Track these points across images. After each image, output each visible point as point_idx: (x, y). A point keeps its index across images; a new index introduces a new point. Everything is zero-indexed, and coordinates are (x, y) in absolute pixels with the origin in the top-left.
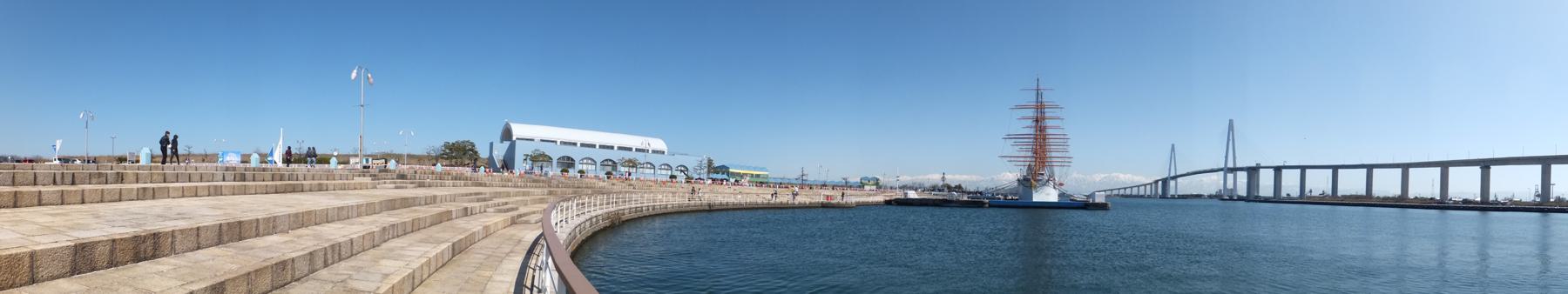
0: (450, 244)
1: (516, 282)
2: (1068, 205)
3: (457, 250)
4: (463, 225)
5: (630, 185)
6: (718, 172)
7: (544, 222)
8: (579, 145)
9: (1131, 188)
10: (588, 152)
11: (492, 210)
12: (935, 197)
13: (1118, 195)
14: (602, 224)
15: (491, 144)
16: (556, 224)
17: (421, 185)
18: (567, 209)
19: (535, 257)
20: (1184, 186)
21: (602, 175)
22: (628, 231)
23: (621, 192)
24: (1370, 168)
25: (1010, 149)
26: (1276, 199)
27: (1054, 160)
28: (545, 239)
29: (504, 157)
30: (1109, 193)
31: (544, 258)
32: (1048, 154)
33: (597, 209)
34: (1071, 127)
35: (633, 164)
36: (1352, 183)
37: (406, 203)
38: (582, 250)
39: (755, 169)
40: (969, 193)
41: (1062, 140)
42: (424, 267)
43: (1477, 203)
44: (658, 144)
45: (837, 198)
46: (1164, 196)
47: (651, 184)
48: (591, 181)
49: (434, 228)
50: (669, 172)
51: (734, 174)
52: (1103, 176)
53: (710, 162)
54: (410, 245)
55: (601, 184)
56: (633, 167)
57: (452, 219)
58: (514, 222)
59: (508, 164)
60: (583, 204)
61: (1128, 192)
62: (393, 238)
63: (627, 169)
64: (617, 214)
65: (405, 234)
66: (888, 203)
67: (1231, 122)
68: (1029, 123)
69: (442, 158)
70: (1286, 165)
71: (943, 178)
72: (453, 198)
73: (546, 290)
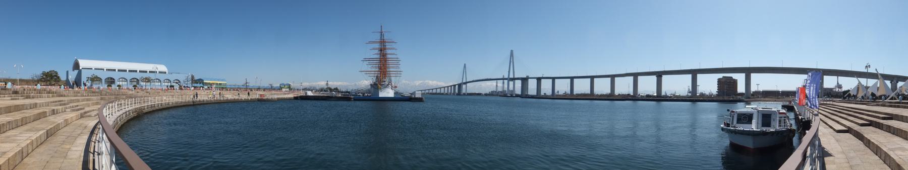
0: (45, 131)
1: (85, 150)
2: (400, 99)
3: (50, 134)
4: (52, 120)
5: (147, 92)
6: (197, 82)
7: (100, 114)
8: (117, 71)
9: (436, 89)
10: (122, 74)
11: (69, 110)
12: (322, 95)
13: (428, 93)
14: (132, 115)
15: (67, 72)
16: (106, 116)
17: (28, 97)
18: (112, 108)
19: (95, 135)
20: (471, 88)
21: (131, 87)
22: (146, 120)
23: (142, 97)
24: (592, 78)
25: (366, 67)
26: (538, 96)
27: (391, 73)
28: (101, 124)
29: (75, 80)
30: (423, 92)
31: (101, 135)
32: (388, 70)
33: (129, 107)
34: (399, 52)
35: (148, 80)
36: (582, 87)
37: (18, 108)
38: (122, 129)
39: (218, 80)
40: (342, 92)
42: (29, 146)
43: (654, 96)
44: (162, 68)
45: (269, 95)
46: (459, 94)
47: (159, 91)
48: (124, 91)
49: (35, 122)
50: (169, 84)
51: (206, 84)
52: (420, 82)
53: (193, 77)
54: (20, 133)
55: (130, 92)
56: (148, 82)
57: (46, 117)
58: (82, 116)
59: (78, 82)
60: (121, 104)
61: (434, 91)
62: (10, 130)
63: (144, 83)
64: (140, 109)
65: (17, 127)
66: (296, 98)
67: (512, 52)
68: (377, 51)
69: (42, 81)
70: (544, 76)
71: (327, 84)
72: (47, 104)
73: (103, 153)
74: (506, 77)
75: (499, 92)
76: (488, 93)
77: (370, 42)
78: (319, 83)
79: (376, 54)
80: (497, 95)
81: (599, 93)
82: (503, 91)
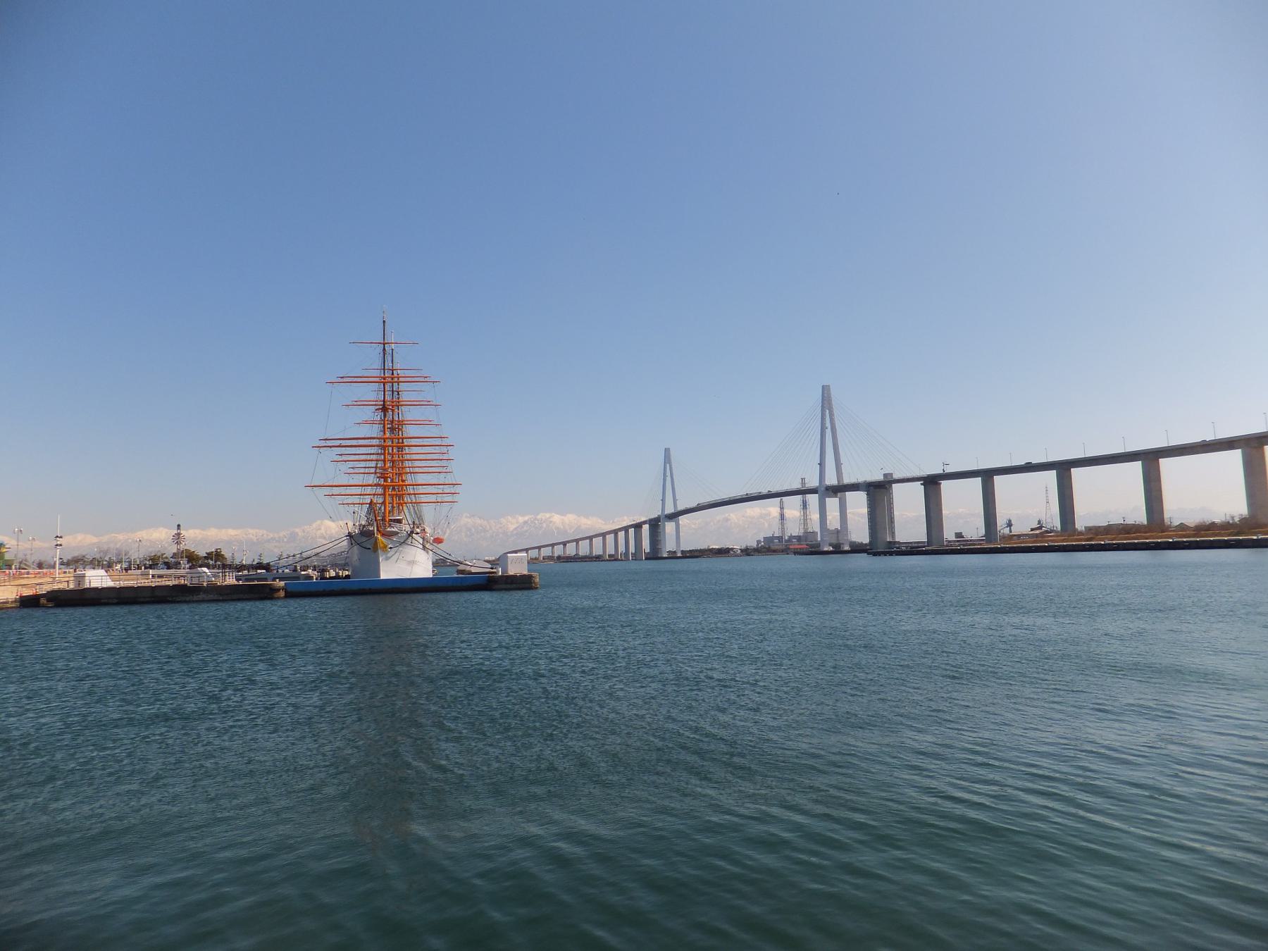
9: (577, 541)
13: (551, 558)
20: (675, 537)
24: (1064, 469)
25: (329, 469)
26: (934, 547)
27: (421, 489)
30: (534, 554)
32: (409, 479)
40: (241, 568)
41: (437, 450)
46: (654, 555)
52: (521, 519)
61: (571, 550)
66: (29, 603)
68: (370, 413)
70: (949, 470)
71: (178, 538)
74: (813, 482)
75: (791, 537)
76: (755, 545)
77: (343, 380)
78: (143, 534)
79: (366, 422)
80: (786, 551)
81: (1192, 520)
82: (806, 533)
